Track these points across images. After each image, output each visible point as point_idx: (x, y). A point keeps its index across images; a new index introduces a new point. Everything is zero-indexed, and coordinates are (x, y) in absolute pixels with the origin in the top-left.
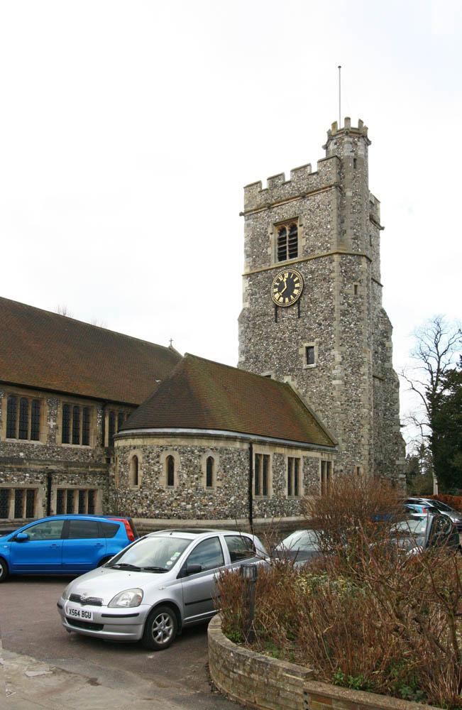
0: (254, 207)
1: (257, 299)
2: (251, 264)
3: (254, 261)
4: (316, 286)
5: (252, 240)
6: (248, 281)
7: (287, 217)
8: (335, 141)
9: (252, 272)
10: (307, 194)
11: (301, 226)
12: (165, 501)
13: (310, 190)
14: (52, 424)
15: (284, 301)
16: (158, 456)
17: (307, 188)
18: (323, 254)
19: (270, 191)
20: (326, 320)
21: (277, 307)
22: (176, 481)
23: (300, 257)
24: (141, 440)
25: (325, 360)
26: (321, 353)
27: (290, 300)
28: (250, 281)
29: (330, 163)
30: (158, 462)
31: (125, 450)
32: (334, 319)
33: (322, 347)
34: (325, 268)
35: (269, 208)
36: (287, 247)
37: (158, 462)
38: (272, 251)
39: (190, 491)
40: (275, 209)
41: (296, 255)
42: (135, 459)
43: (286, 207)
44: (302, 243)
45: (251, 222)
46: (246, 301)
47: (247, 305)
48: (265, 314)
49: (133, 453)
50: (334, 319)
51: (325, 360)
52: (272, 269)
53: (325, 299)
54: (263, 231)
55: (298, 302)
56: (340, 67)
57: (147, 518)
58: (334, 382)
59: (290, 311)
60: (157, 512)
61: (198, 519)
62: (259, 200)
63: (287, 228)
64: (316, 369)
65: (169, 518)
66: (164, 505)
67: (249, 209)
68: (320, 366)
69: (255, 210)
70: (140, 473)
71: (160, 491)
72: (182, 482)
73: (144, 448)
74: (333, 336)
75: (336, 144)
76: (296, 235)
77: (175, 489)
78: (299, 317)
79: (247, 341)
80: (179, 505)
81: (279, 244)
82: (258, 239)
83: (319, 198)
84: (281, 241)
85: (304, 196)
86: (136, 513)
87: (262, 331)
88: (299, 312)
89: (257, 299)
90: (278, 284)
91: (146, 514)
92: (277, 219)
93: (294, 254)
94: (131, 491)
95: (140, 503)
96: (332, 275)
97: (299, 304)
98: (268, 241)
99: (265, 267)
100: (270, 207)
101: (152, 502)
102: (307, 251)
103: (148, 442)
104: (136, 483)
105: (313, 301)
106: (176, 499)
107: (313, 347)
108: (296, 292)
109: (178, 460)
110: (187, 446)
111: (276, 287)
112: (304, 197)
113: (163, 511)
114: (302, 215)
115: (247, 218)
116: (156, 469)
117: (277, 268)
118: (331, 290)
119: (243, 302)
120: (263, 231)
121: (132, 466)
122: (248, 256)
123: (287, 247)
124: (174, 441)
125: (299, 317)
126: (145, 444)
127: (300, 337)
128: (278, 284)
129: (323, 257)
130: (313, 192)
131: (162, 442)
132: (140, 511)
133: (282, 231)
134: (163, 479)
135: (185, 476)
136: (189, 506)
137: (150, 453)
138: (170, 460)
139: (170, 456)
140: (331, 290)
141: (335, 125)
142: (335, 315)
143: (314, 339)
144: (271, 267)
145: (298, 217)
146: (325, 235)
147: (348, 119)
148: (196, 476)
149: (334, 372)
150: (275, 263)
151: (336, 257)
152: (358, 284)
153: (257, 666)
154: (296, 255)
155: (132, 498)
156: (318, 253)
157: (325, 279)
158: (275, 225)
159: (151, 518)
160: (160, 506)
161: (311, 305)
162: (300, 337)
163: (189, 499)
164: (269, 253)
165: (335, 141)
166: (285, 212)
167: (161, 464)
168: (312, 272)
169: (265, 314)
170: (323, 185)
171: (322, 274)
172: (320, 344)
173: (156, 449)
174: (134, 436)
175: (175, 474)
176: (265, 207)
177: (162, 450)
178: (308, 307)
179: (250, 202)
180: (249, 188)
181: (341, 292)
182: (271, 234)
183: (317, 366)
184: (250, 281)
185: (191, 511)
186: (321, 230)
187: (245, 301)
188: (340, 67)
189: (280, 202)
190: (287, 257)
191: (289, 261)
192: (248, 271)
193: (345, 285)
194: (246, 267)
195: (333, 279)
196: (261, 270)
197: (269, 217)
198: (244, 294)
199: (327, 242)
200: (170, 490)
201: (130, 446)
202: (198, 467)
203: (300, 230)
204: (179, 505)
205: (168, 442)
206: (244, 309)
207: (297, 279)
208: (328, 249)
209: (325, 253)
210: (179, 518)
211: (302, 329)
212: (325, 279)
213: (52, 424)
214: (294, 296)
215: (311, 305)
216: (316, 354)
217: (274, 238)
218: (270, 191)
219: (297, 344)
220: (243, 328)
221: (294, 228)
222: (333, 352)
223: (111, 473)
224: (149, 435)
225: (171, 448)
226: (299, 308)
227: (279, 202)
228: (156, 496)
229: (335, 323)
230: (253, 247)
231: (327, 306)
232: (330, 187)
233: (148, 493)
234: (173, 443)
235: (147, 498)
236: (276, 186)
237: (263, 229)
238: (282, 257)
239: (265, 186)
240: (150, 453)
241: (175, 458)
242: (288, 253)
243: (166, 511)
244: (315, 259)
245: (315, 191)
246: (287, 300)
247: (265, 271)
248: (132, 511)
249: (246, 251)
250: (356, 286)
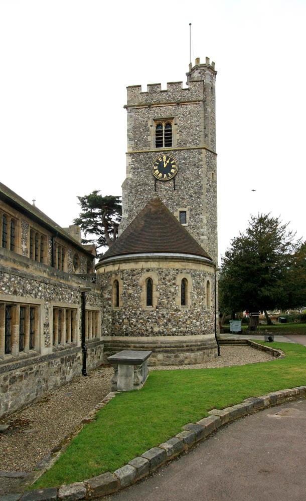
0: (136, 104)
1: (139, 173)
2: (133, 146)
3: (136, 144)
4: (188, 169)
5: (134, 128)
6: (131, 158)
7: (164, 116)
8: (199, 71)
9: (134, 152)
10: (181, 103)
11: (176, 124)
12: (181, 320)
13: (182, 100)
14: (24, 247)
15: (163, 176)
16: (174, 279)
17: (181, 99)
18: (193, 147)
19: (150, 95)
20: (195, 193)
21: (156, 180)
22: (189, 301)
23: (174, 145)
24: (156, 263)
25: (195, 221)
26: (191, 217)
27: (168, 176)
28: (133, 158)
29: (199, 85)
30: (174, 284)
31: (133, 273)
32: (202, 194)
33: (193, 212)
34: (195, 158)
35: (149, 107)
36: (164, 137)
37: (174, 284)
38: (152, 139)
39: (199, 310)
40: (154, 109)
41: (170, 145)
42: (149, 282)
43: (163, 109)
44: (175, 137)
45: (133, 114)
46: (129, 173)
47: (131, 176)
48: (146, 185)
49: (146, 275)
50: (202, 194)
51: (195, 221)
52: (153, 152)
53: (195, 179)
54: (144, 123)
55: (174, 179)
56: (190, 24)
57: (165, 335)
58: (202, 237)
59: (166, 184)
60: (174, 329)
61: (204, 334)
62: (141, 99)
63: (164, 125)
64: (188, 227)
65: (184, 335)
66: (180, 323)
67: (132, 104)
68: (191, 225)
69: (164, 104)
70: (155, 294)
71: (177, 310)
72: (193, 302)
73: (160, 271)
74: (201, 205)
75: (200, 73)
76: (171, 131)
77: (189, 308)
78: (175, 190)
79: (130, 203)
80: (191, 322)
81: (157, 135)
82: (139, 128)
83: (190, 107)
84: (158, 133)
85: (178, 104)
86: (152, 332)
87: (144, 197)
88: (175, 186)
89: (139, 173)
90: (158, 163)
91: (163, 332)
92: (156, 116)
93: (169, 144)
94: (144, 311)
95: (156, 322)
96: (201, 163)
97: (174, 180)
98: (148, 131)
99: (145, 150)
100: (150, 106)
101: (169, 320)
102: (181, 144)
103: (164, 265)
104: (150, 302)
105: (187, 180)
106: (189, 317)
107: (185, 212)
108: (172, 171)
109: (191, 282)
110: (196, 270)
111: (155, 165)
112: (178, 104)
113: (179, 328)
114: (177, 117)
115: (129, 111)
116: (173, 291)
117: (156, 152)
118: (200, 173)
119: (127, 173)
120: (144, 123)
121: (145, 288)
122: (130, 139)
123: (164, 137)
124: (187, 265)
125: (175, 190)
126: (161, 267)
127: (175, 204)
128: (158, 163)
129: (193, 149)
130: (185, 102)
131: (178, 265)
132: (156, 329)
133: (159, 126)
134: (179, 299)
135: (196, 296)
136: (198, 323)
137: (166, 275)
138: (184, 281)
139: (185, 278)
140: (200, 173)
141: (190, 65)
142: (202, 191)
143: (186, 206)
144: (151, 150)
145: (174, 118)
146: (195, 135)
147: (198, 60)
148: (202, 297)
149: (202, 230)
150: (153, 148)
151: (203, 151)
152: (214, 172)
153: (2, 438)
154: (170, 145)
155: (145, 318)
156: (189, 146)
157: (195, 165)
158: (155, 120)
159: (169, 335)
160: (176, 325)
161: (184, 182)
162: (175, 204)
163: (198, 317)
164: (149, 140)
165: (199, 71)
166: (165, 112)
167: (177, 286)
168: (185, 159)
169: (146, 185)
170: (194, 100)
171: (193, 162)
172: (191, 210)
173: (172, 272)
174: (148, 259)
175: (189, 295)
176: (146, 105)
177: (177, 273)
178: (182, 183)
179: (132, 99)
180: (131, 88)
181: (206, 176)
182: (151, 126)
183: (189, 225)
184: (133, 158)
185: (200, 327)
186: (192, 130)
187: (128, 172)
188: (190, 24)
189: (159, 104)
190: (164, 145)
191: (164, 148)
192: (131, 150)
193: (208, 172)
194: (129, 148)
195: (201, 165)
196: (142, 151)
197: (149, 113)
198: (127, 167)
199: (196, 139)
200: (185, 309)
201: (142, 269)
202: (202, 289)
203: (174, 127)
204: (191, 322)
205: (182, 266)
206: (127, 179)
207: (173, 162)
208: (197, 144)
209: (195, 146)
210: (192, 334)
211: (176, 198)
212: (195, 165)
213: (24, 247)
214: (171, 173)
215: (184, 182)
216: (188, 217)
217: (153, 129)
218: (150, 95)
219: (173, 208)
220: (126, 193)
221: (169, 125)
222: (201, 216)
223: (106, 296)
224: (166, 258)
225: (185, 271)
226: (174, 183)
227: (158, 104)
228: (172, 315)
229: (202, 197)
230: (135, 133)
231: (196, 184)
232: (199, 101)
233: (165, 313)
234: (187, 267)
235: (164, 317)
236: (155, 92)
237: (144, 121)
238: (159, 144)
239: (145, 89)
240: (166, 275)
241: (188, 280)
242: (164, 143)
243: (182, 328)
244: (187, 149)
245: (187, 102)
246: (165, 176)
247: (146, 152)
248: (147, 330)
249: (128, 135)
250: (213, 174)
